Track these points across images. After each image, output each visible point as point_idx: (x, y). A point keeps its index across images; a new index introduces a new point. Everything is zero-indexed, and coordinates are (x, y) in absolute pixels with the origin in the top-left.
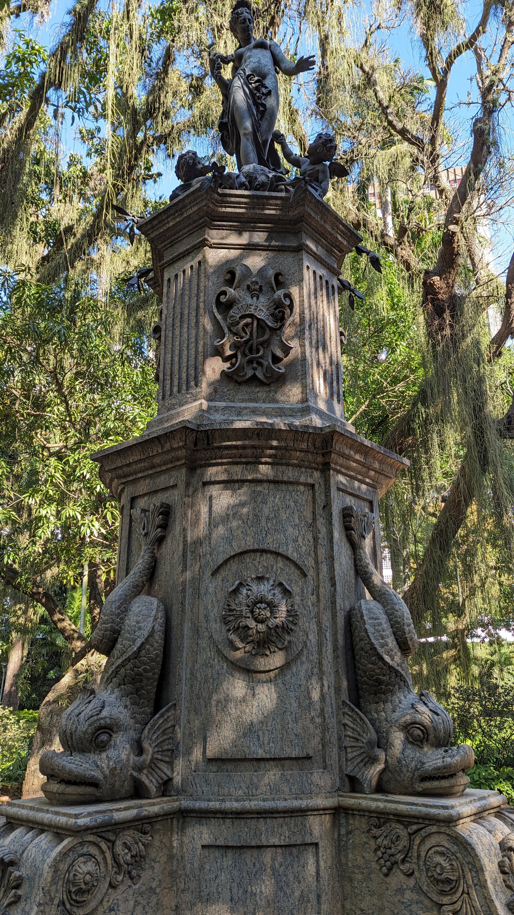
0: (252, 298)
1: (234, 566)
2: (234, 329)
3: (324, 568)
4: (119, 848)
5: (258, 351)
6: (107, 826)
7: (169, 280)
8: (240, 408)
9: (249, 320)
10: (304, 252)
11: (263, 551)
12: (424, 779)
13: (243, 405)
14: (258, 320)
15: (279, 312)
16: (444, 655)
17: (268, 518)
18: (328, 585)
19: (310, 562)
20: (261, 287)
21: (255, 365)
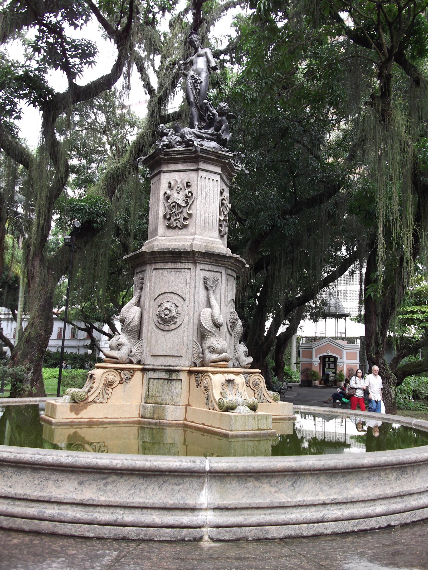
1: (161, 297)
3: (192, 298)
4: (122, 374)
6: (182, 475)
9: (174, 204)
11: (170, 293)
12: (212, 362)
14: (178, 204)
17: (172, 282)
18: (193, 303)
19: (187, 296)
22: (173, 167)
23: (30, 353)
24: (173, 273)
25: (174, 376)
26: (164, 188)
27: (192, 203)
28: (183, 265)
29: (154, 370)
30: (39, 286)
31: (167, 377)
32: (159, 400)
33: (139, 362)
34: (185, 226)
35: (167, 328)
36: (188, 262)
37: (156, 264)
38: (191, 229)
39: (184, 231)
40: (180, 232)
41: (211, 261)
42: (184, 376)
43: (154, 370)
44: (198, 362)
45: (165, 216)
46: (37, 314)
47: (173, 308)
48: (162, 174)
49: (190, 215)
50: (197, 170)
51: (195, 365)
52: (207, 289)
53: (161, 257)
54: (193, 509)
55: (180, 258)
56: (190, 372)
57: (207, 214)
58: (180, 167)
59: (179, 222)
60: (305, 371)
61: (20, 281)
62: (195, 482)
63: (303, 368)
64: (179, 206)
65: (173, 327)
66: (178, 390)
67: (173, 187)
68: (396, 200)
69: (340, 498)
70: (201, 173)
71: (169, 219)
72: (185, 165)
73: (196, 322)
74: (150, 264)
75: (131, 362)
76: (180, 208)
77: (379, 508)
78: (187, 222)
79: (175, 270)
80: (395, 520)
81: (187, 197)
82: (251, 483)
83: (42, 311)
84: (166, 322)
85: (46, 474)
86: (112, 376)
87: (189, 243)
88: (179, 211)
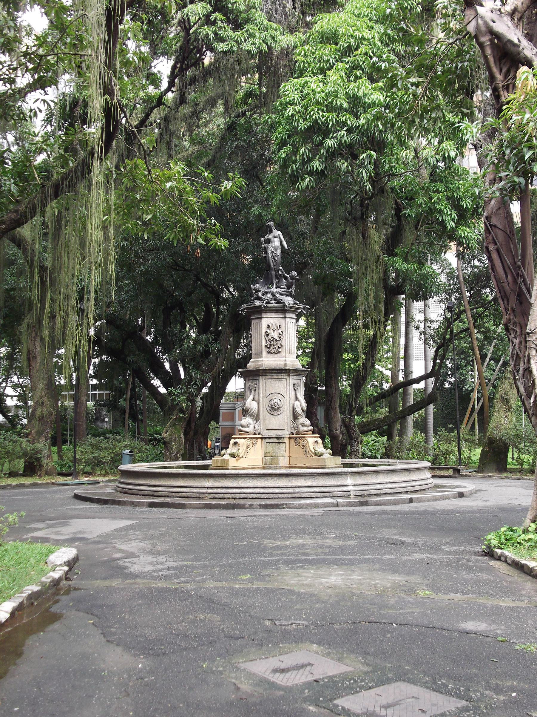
22: (269, 315)
23: (45, 430)
24: (277, 381)
25: (281, 441)
26: (264, 329)
28: (282, 377)
29: (269, 438)
30: (40, 365)
31: (277, 441)
32: (274, 455)
33: (259, 434)
34: (279, 352)
35: (276, 414)
38: (283, 354)
39: (278, 355)
40: (276, 356)
42: (286, 441)
43: (269, 438)
44: (294, 432)
45: (266, 346)
46: (43, 393)
47: (279, 401)
49: (282, 345)
50: (285, 317)
51: (293, 434)
52: (295, 390)
54: (346, 486)
55: (281, 373)
56: (290, 438)
58: (273, 315)
60: (226, 437)
62: (345, 476)
63: (224, 433)
64: (276, 340)
65: (279, 413)
66: (284, 448)
68: (372, 295)
69: (391, 481)
70: (287, 320)
71: (269, 348)
73: (291, 409)
74: (262, 376)
75: (255, 434)
77: (404, 485)
78: (280, 350)
80: (409, 489)
81: (280, 334)
82: (363, 476)
83: (48, 390)
84: (275, 410)
85: (291, 478)
86: (249, 443)
87: (283, 363)
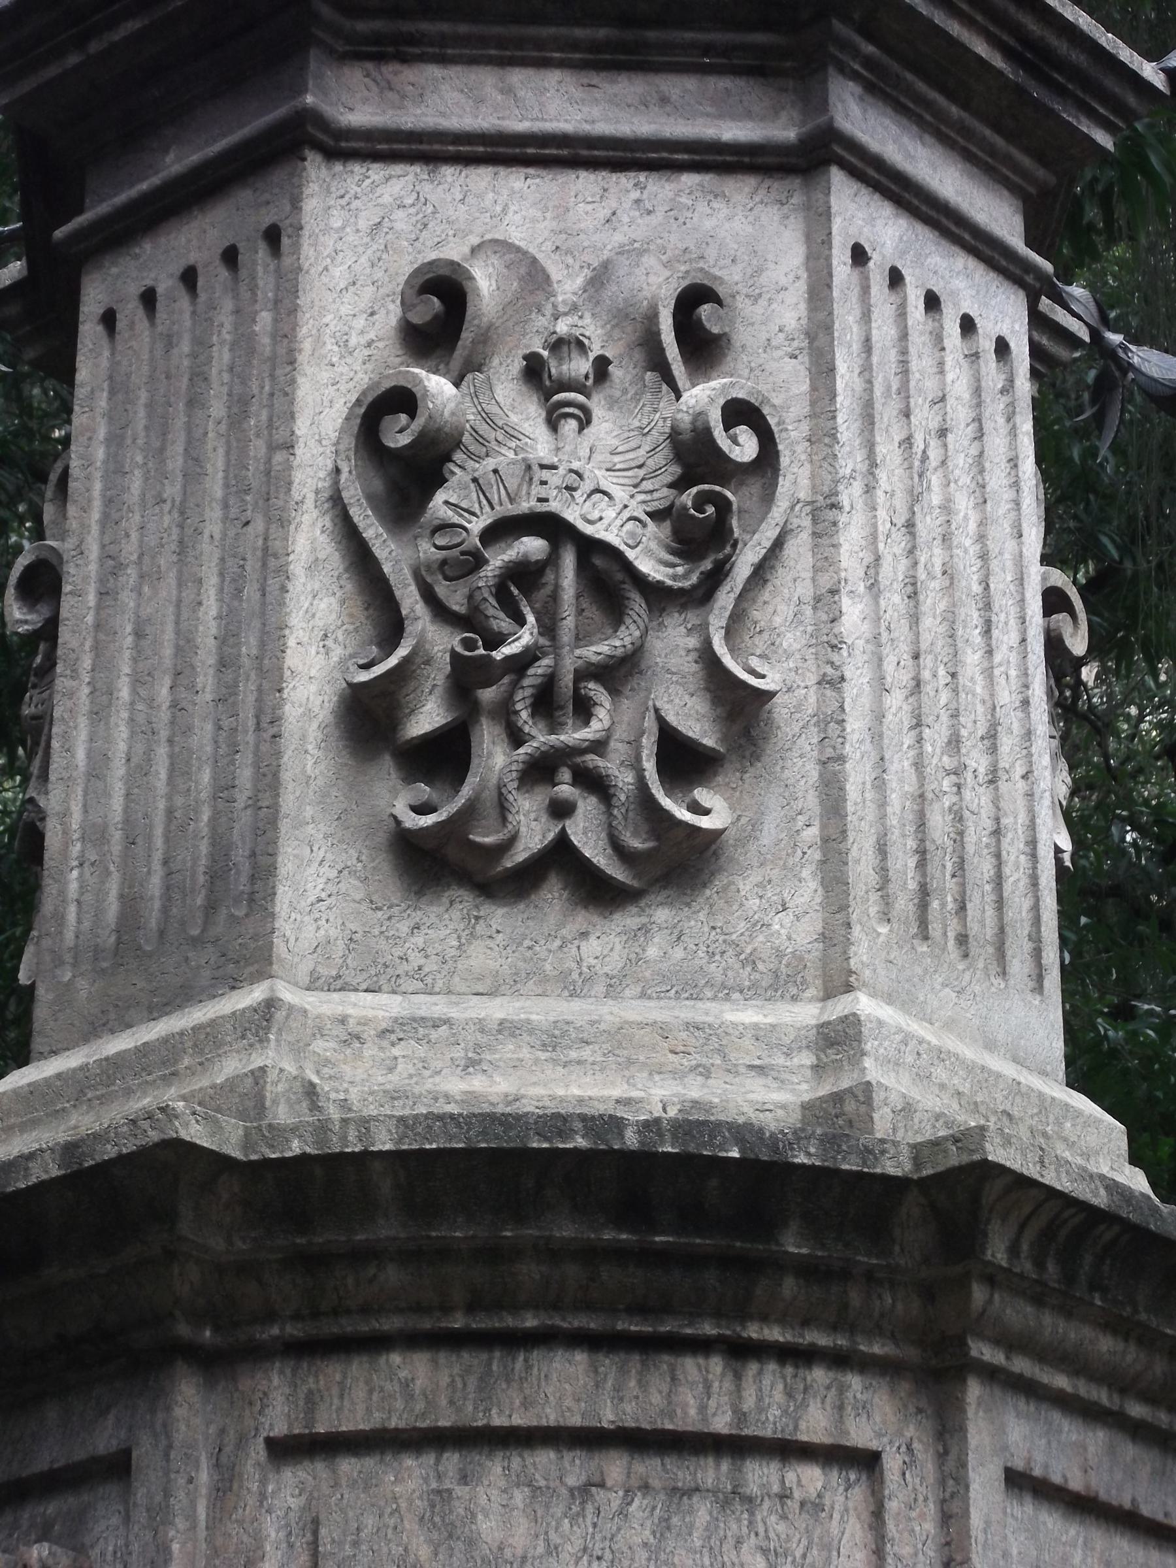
0: (553, 424)
2: (455, 598)
5: (584, 710)
7: (109, 319)
8: (481, 1026)
9: (532, 546)
10: (837, 176)
13: (497, 1009)
14: (589, 548)
15: (701, 502)
16: (1140, 928)
20: (602, 366)
21: (565, 790)
27: (761, 573)
36: (840, 1360)
37: (332, 1371)
41: (1131, 1356)
48: (315, 171)
53: (444, 1253)
57: (936, 735)
59: (587, 807)
61: (486, 79)
67: (485, 338)
72: (629, 87)
76: (616, 613)
79: (651, 1467)
88: (598, 650)
